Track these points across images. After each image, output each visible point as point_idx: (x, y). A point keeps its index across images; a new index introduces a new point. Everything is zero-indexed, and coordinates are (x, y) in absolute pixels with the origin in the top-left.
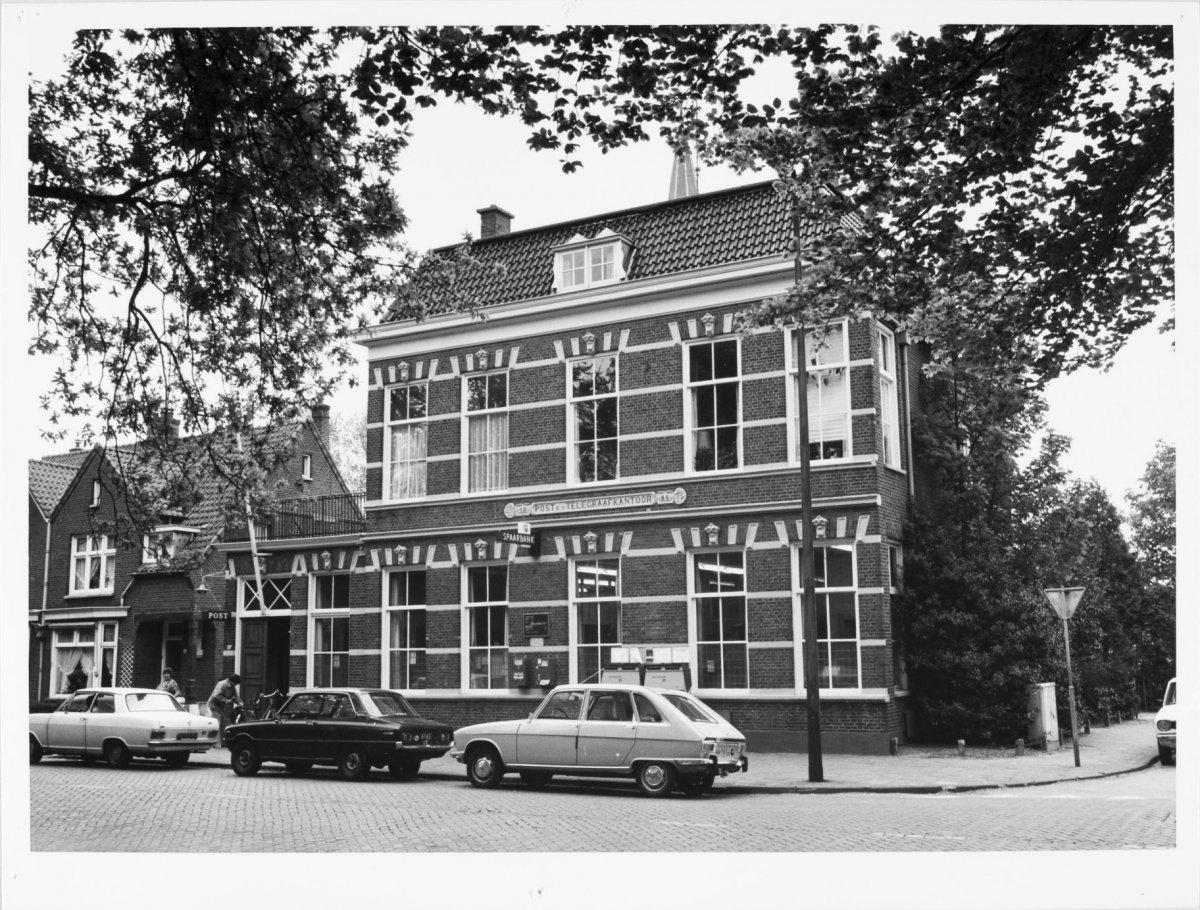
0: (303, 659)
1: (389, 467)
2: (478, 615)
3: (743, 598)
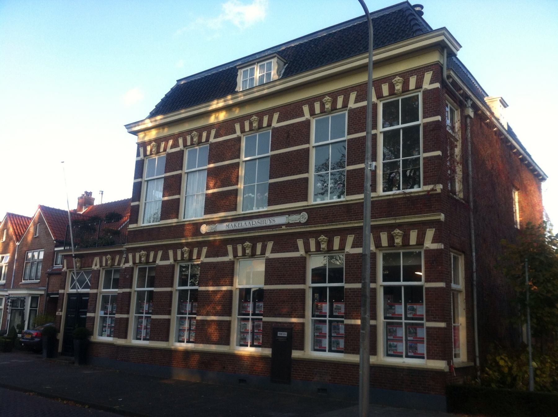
0: (93, 319)
1: (144, 204)
2: (388, 291)
3: (421, 287)
